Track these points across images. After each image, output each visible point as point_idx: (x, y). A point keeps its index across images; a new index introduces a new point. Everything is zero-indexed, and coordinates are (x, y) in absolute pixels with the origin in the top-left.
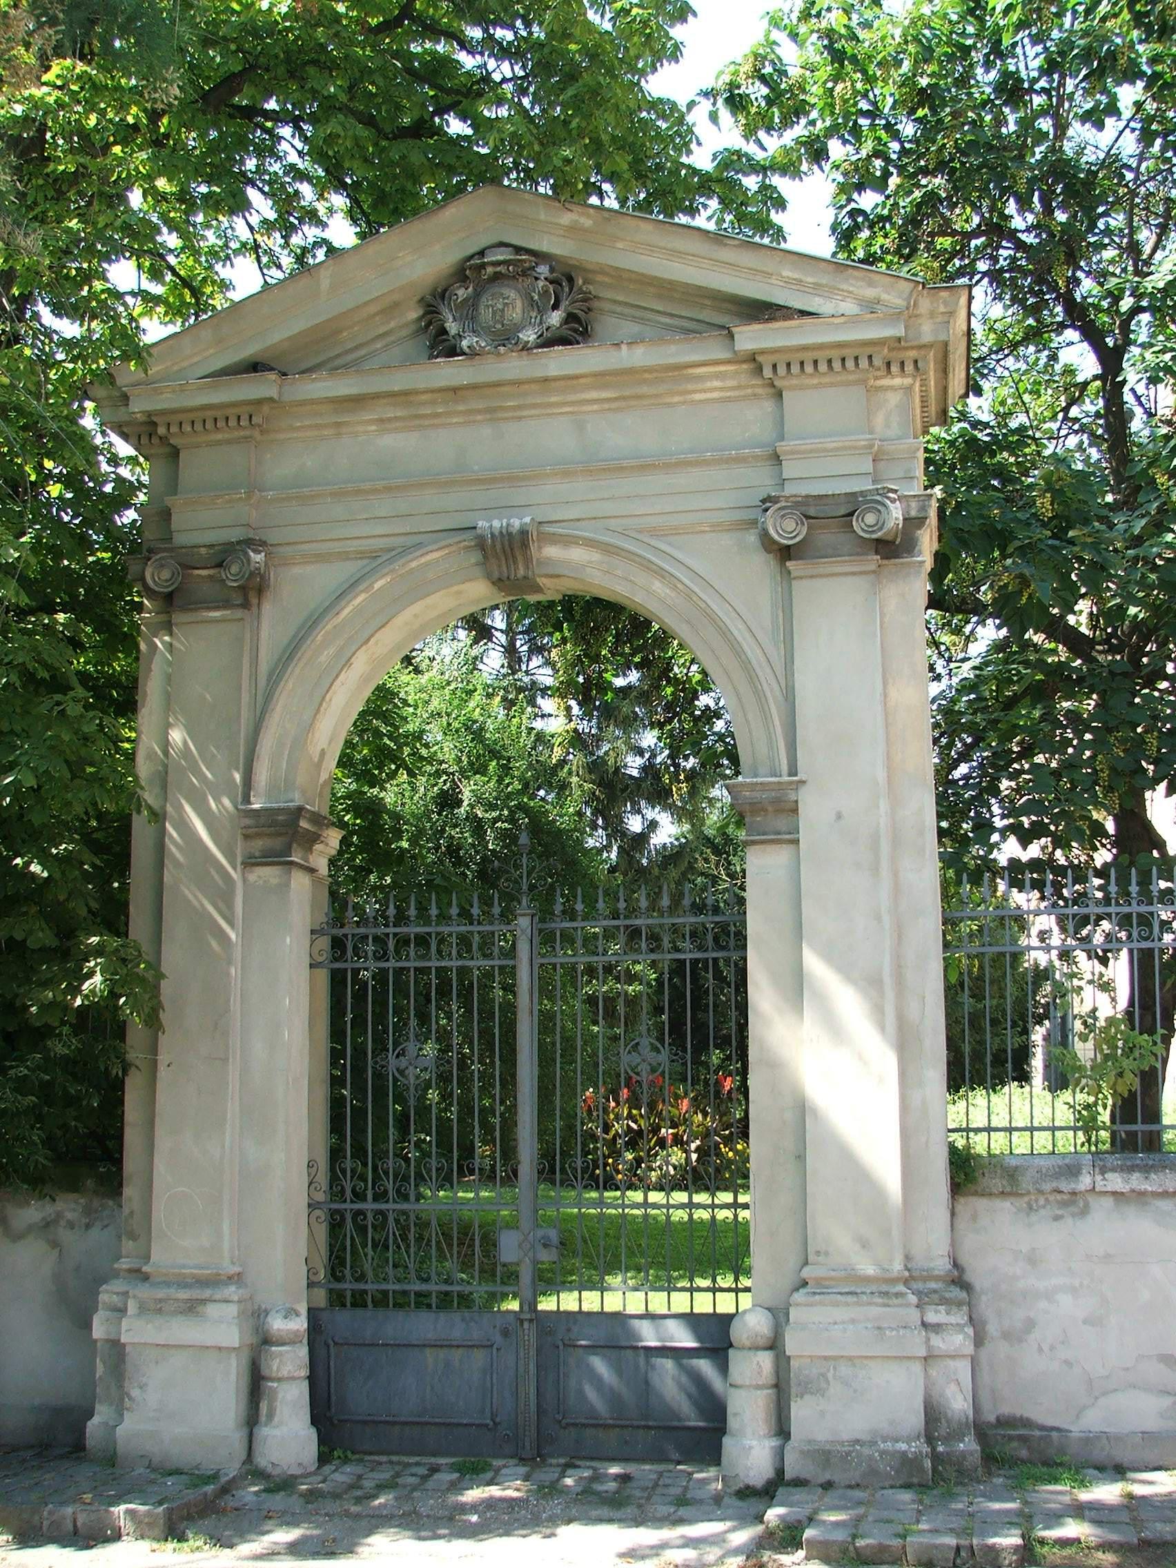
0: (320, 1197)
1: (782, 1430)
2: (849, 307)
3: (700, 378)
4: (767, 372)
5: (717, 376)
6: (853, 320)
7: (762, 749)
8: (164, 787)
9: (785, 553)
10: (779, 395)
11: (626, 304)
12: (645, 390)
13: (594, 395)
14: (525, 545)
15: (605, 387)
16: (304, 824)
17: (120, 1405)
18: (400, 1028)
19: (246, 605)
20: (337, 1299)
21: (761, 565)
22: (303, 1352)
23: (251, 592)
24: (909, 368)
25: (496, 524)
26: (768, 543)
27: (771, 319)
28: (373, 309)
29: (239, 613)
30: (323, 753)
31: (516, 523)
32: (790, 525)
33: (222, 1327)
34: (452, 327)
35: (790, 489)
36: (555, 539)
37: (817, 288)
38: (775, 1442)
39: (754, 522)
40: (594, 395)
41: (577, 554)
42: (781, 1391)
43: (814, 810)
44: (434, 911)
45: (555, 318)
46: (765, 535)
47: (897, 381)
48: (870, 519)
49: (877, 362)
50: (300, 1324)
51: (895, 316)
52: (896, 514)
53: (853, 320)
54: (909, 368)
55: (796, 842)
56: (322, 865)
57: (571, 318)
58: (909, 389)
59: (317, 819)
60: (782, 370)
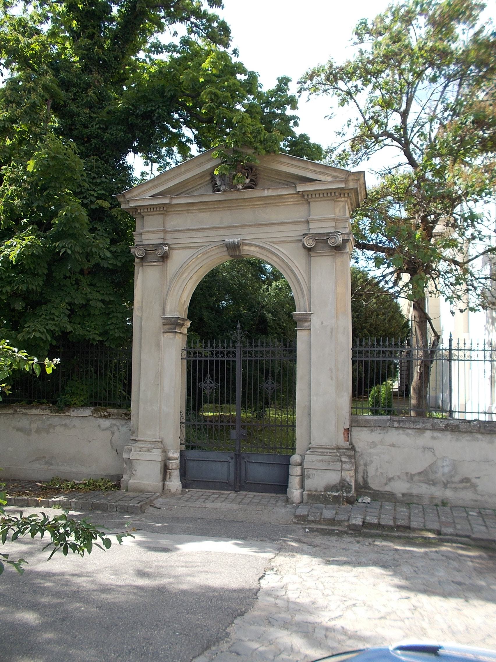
0: (184, 421)
1: (302, 487)
2: (329, 179)
3: (288, 198)
4: (306, 197)
5: (291, 198)
6: (331, 182)
7: (302, 304)
8: (142, 310)
9: (309, 250)
10: (309, 203)
11: (154, 232)
12: (272, 202)
13: (258, 203)
14: (238, 247)
15: (262, 200)
16: (179, 321)
17: (132, 475)
18: (205, 375)
19: (163, 261)
20: (187, 447)
21: (303, 252)
22: (178, 462)
23: (165, 258)
24: (346, 195)
25: (230, 240)
26: (304, 247)
27: (408, 114)
28: (197, 177)
29: (161, 263)
30: (185, 301)
31: (236, 240)
32: (310, 242)
33: (156, 455)
34: (218, 183)
35: (312, 231)
36: (247, 244)
37: (320, 173)
38: (301, 491)
39: (301, 240)
40: (258, 203)
41: (253, 249)
42: (303, 477)
43: (315, 321)
44: (214, 345)
45: (248, 181)
46: (304, 245)
47: (343, 199)
48: (333, 240)
49: (337, 194)
50: (177, 455)
51: (341, 181)
52: (340, 239)
53: (331, 182)
54: (346, 195)
55: (310, 329)
56: (185, 331)
57: (251, 180)
58: (347, 201)
59: (183, 319)
60: (310, 197)
